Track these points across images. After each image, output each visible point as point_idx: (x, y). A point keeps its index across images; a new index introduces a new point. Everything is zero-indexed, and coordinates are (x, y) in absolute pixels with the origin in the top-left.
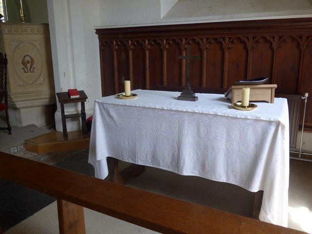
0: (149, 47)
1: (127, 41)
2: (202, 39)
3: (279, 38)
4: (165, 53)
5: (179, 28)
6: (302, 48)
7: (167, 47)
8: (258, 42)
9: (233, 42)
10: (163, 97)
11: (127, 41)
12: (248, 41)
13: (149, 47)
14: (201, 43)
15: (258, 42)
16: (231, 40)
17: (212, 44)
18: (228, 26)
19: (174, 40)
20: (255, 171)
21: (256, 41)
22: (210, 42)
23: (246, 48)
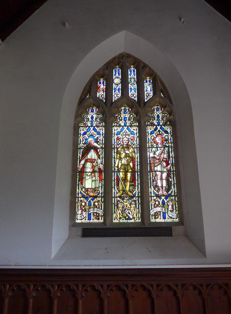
0: (34, 294)
1: (4, 285)
2: (53, 286)
3: (182, 286)
4: (56, 302)
5: (77, 273)
6: (204, 296)
7: (59, 294)
8: (162, 290)
9: (137, 290)
10: (168, 129)
11: (4, 285)
12: (211, 284)
13: (10, 294)
14: (101, 290)
15: (162, 290)
16: (85, 288)
17: (113, 291)
18: (229, 269)
19: (68, 286)
20: (72, 188)
21: (85, 289)
22: (87, 290)
23: (150, 295)
